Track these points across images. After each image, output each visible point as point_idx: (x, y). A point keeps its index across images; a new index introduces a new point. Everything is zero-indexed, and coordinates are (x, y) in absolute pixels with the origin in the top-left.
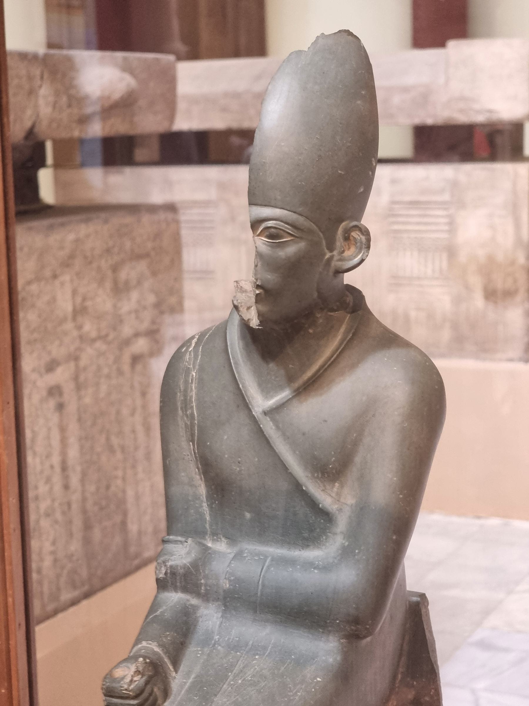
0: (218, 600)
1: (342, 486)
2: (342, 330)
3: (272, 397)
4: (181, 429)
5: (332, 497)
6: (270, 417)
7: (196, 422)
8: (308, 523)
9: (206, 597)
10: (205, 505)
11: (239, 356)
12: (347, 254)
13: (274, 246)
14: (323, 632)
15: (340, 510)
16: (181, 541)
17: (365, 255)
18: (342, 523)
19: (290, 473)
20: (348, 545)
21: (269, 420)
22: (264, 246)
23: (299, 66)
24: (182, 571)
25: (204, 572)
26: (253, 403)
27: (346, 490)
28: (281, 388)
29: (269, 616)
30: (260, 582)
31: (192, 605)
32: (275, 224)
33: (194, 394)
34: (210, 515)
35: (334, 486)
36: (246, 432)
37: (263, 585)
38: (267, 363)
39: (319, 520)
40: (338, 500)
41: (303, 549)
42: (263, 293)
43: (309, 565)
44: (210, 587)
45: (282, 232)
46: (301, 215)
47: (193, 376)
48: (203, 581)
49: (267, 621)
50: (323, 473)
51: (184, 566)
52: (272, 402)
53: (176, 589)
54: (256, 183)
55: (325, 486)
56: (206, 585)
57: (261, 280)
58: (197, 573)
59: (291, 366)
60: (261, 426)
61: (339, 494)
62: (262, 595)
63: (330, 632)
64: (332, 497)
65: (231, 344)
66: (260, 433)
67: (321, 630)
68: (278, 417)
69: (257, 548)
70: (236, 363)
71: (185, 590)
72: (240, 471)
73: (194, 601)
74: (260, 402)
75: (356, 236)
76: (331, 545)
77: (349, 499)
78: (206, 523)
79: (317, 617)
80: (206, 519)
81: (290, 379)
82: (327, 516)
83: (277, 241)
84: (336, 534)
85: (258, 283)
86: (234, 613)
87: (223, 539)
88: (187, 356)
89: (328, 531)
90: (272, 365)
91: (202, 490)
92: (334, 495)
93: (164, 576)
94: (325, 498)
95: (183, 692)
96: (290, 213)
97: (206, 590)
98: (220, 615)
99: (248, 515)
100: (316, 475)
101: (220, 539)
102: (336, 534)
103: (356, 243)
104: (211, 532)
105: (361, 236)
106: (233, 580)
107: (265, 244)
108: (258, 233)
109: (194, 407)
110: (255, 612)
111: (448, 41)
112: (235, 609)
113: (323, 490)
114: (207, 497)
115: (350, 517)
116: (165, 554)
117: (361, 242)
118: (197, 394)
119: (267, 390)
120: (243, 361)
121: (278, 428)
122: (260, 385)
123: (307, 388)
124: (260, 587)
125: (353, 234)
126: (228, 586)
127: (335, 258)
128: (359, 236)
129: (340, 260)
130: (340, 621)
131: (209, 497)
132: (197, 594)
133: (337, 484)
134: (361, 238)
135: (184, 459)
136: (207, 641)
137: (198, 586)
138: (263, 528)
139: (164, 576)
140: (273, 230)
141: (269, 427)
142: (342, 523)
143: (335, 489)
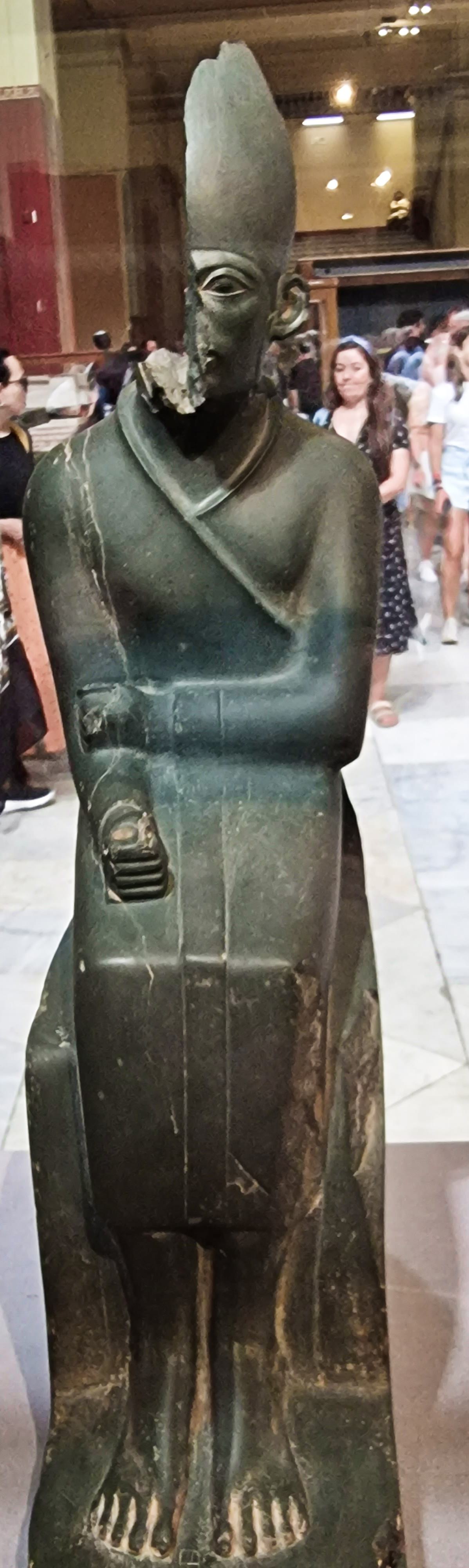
0: (166, 749)
1: (298, 595)
2: (267, 415)
3: (204, 498)
4: (73, 558)
9: (154, 748)
10: (118, 644)
11: (148, 456)
12: (286, 316)
15: (298, 624)
18: (302, 639)
24: (122, 720)
25: (147, 717)
27: (303, 600)
28: (213, 488)
29: (239, 757)
31: (138, 760)
36: (177, 544)
40: (293, 611)
43: (275, 692)
44: (156, 734)
49: (235, 763)
50: (278, 583)
51: (124, 715)
52: (204, 504)
53: (115, 744)
55: (278, 597)
56: (151, 733)
57: (214, 343)
61: (295, 605)
71: (127, 743)
72: (172, 591)
73: (139, 755)
74: (191, 508)
77: (308, 610)
81: (222, 474)
82: (284, 633)
87: (150, 681)
88: (67, 468)
90: (198, 460)
91: (114, 627)
94: (280, 614)
95: (179, 854)
98: (173, 767)
99: (183, 646)
111: (334, 85)
112: (194, 755)
114: (119, 634)
115: (311, 630)
116: (90, 708)
118: (98, 506)
119: (195, 495)
121: (216, 532)
122: (184, 485)
123: (241, 487)
125: (292, 290)
132: (142, 747)
133: (292, 594)
136: (170, 796)
138: (208, 656)
141: (205, 533)
142: (302, 639)
143: (290, 600)
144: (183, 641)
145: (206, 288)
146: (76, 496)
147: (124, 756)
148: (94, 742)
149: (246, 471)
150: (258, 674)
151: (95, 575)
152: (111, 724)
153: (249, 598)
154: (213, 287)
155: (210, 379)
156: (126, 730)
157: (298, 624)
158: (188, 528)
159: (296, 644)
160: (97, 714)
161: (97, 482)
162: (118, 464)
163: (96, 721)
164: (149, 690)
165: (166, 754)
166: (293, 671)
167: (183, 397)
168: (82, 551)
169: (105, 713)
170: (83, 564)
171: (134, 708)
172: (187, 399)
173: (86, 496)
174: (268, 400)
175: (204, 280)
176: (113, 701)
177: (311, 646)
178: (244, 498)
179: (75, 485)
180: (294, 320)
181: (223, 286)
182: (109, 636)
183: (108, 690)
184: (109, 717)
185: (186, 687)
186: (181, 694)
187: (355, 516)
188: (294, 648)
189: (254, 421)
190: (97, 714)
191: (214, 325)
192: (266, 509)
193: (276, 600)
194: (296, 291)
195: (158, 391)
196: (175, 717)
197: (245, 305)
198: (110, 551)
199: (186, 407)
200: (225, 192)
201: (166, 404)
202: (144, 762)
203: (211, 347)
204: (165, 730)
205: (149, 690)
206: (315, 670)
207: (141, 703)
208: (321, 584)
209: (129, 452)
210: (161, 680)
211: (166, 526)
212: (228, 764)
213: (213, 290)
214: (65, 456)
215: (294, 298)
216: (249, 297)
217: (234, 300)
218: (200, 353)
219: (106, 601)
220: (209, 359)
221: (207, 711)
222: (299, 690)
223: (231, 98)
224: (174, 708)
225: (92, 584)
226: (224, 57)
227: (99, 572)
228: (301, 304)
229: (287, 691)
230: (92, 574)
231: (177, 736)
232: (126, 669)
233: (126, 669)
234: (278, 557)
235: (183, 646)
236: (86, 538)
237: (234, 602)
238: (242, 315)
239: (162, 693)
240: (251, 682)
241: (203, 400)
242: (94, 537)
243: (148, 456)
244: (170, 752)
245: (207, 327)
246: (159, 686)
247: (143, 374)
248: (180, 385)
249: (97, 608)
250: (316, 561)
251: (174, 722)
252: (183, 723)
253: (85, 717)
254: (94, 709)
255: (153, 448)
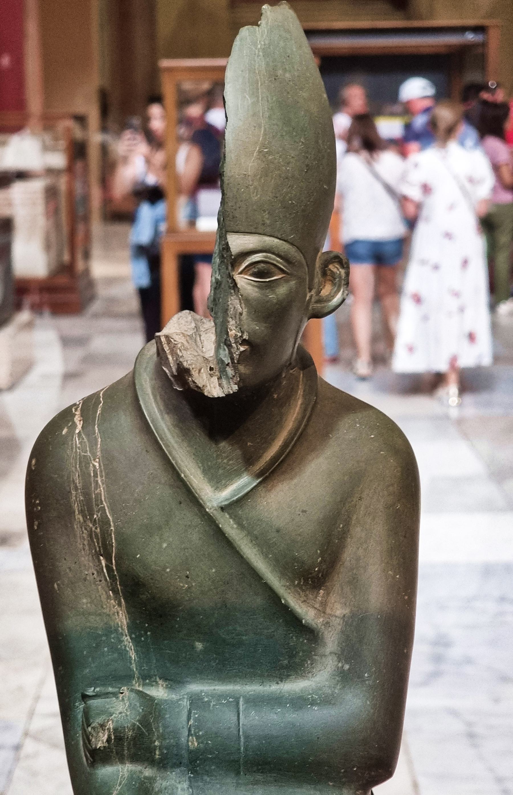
0: (179, 765)
2: (300, 392)
3: (226, 486)
5: (316, 608)
6: (229, 514)
7: (112, 528)
8: (289, 645)
9: (165, 763)
10: (127, 640)
11: (169, 435)
12: (325, 292)
13: (262, 286)
14: (334, 786)
15: (327, 624)
16: (112, 693)
17: (345, 295)
18: (331, 641)
19: (266, 583)
20: (349, 669)
21: (228, 516)
22: (249, 288)
23: (259, 46)
25: (157, 728)
26: (203, 497)
27: (333, 598)
28: (238, 474)
29: (259, 777)
30: (241, 733)
31: (146, 778)
32: (265, 257)
33: (102, 489)
34: (136, 651)
35: (318, 593)
36: (196, 536)
37: (247, 737)
38: (217, 442)
39: (301, 640)
40: (322, 610)
41: (282, 681)
42: (249, 349)
43: (300, 702)
45: (272, 267)
46: (292, 244)
47: (94, 466)
48: (157, 743)
49: (256, 783)
50: (306, 580)
53: (122, 761)
54: (236, 203)
55: (306, 596)
57: (249, 334)
58: (149, 734)
59: (249, 444)
60: (220, 526)
61: (324, 604)
62: (246, 749)
63: (344, 784)
64: (316, 608)
65: (153, 422)
66: (219, 534)
67: (331, 784)
68: (240, 512)
69: (217, 688)
70: (167, 446)
71: (135, 759)
72: (189, 588)
73: (148, 772)
74: (214, 497)
75: (335, 270)
76: (320, 671)
77: (339, 610)
78: (131, 663)
79: (326, 768)
80: (130, 657)
81: (249, 460)
82: (311, 634)
83: (268, 280)
84: (325, 656)
85: (244, 337)
86: (208, 779)
87: (160, 682)
89: (313, 653)
91: (122, 619)
92: (317, 606)
93: (106, 745)
94: (307, 613)
96: (282, 242)
97: (161, 754)
98: (185, 785)
99: (199, 646)
100: (296, 582)
101: (157, 682)
102: (325, 656)
103: (335, 279)
104: (140, 674)
105: (340, 270)
106: (203, 735)
107: (254, 286)
108: (240, 270)
109: (106, 508)
110: (238, 773)
112: (208, 773)
113: (305, 601)
115: (342, 632)
117: (340, 277)
118: (108, 491)
119: (218, 478)
120: (176, 442)
121: (241, 526)
124: (242, 739)
125: (331, 267)
126: (196, 744)
127: (313, 300)
128: (338, 270)
129: (319, 301)
130: (358, 768)
131: (133, 628)
132: (152, 762)
133: (322, 592)
134: (340, 272)
135: (85, 579)
137: (151, 750)
138: (226, 657)
139: (106, 745)
140: (262, 265)
141: (229, 526)
142: (331, 641)
144: (199, 641)
145: (241, 273)
146: (85, 475)
147: (131, 777)
148: (98, 757)
149: (275, 459)
150: (282, 678)
151: (103, 563)
152: (118, 737)
153: (274, 597)
154: (251, 272)
155: (242, 368)
156: (135, 745)
157: (327, 624)
158: (210, 521)
159: (325, 645)
160: (102, 726)
161: (108, 459)
162: (131, 440)
163: (101, 734)
164: (159, 692)
165: (178, 770)
166: (319, 678)
167: (211, 376)
168: (90, 535)
169: (111, 725)
170: (90, 549)
171: (145, 721)
172: (215, 379)
173: (96, 476)
174: (302, 372)
175: (240, 264)
176: (119, 709)
177: (343, 651)
178: (273, 486)
179: (85, 462)
180: (333, 297)
181: (261, 272)
182: (116, 630)
183: (115, 695)
184: (115, 730)
185: (202, 691)
186: (196, 701)
187: (393, 505)
188: (321, 650)
189: (287, 400)
190: (102, 726)
191: (249, 313)
192: (296, 500)
193: (310, 675)
194: (335, 268)
195: (183, 373)
196: (190, 730)
197: (282, 290)
198: (122, 541)
199: (214, 388)
200: (266, 173)
201: (192, 385)
202: (151, 780)
203: (246, 337)
204: (178, 745)
205: (159, 692)
206: (345, 678)
207: (152, 709)
208: (354, 582)
209: (145, 427)
210: (174, 681)
211: (186, 516)
212: (246, 784)
213: (251, 275)
214: (74, 426)
215: (333, 273)
216: (287, 281)
217: (271, 286)
218: (232, 340)
219: (115, 592)
220: (242, 349)
221: (225, 719)
222: (327, 701)
223: (275, 69)
224: (189, 719)
225: (100, 571)
226: (267, 24)
227: (108, 559)
228: (340, 281)
229: (313, 703)
230: (100, 561)
231: (190, 752)
232: (134, 666)
233: (134, 666)
234: (310, 555)
235: (199, 646)
236: (94, 522)
237: (259, 601)
238: (280, 303)
239: (174, 697)
240: (274, 688)
241: (235, 388)
242: (104, 522)
243: (169, 435)
244: (183, 768)
245: (241, 314)
246: (170, 688)
247: (166, 348)
248: (206, 360)
249: (104, 597)
250: (348, 555)
251: (188, 736)
252: (198, 737)
253: (90, 729)
254: (99, 720)
255: (176, 426)
